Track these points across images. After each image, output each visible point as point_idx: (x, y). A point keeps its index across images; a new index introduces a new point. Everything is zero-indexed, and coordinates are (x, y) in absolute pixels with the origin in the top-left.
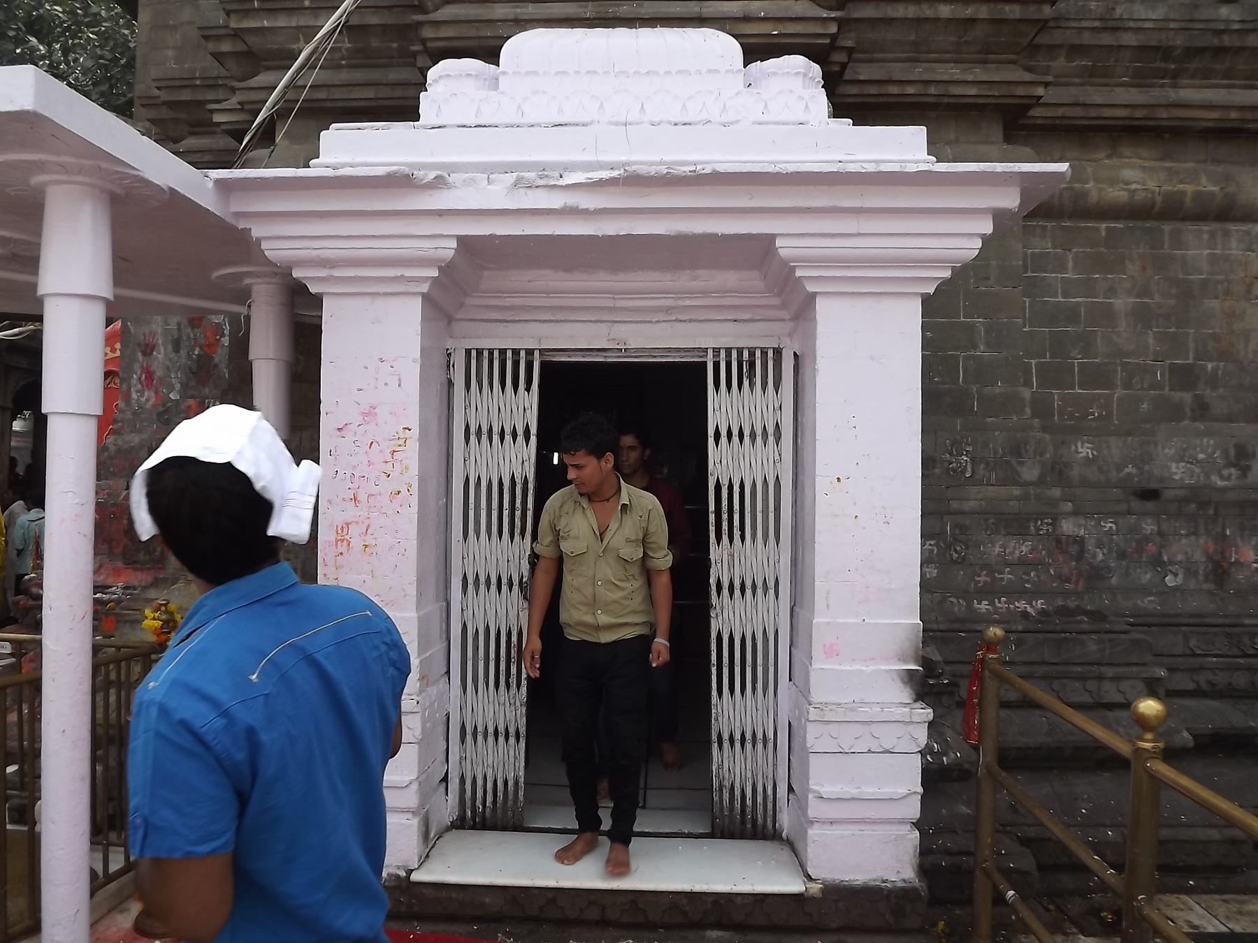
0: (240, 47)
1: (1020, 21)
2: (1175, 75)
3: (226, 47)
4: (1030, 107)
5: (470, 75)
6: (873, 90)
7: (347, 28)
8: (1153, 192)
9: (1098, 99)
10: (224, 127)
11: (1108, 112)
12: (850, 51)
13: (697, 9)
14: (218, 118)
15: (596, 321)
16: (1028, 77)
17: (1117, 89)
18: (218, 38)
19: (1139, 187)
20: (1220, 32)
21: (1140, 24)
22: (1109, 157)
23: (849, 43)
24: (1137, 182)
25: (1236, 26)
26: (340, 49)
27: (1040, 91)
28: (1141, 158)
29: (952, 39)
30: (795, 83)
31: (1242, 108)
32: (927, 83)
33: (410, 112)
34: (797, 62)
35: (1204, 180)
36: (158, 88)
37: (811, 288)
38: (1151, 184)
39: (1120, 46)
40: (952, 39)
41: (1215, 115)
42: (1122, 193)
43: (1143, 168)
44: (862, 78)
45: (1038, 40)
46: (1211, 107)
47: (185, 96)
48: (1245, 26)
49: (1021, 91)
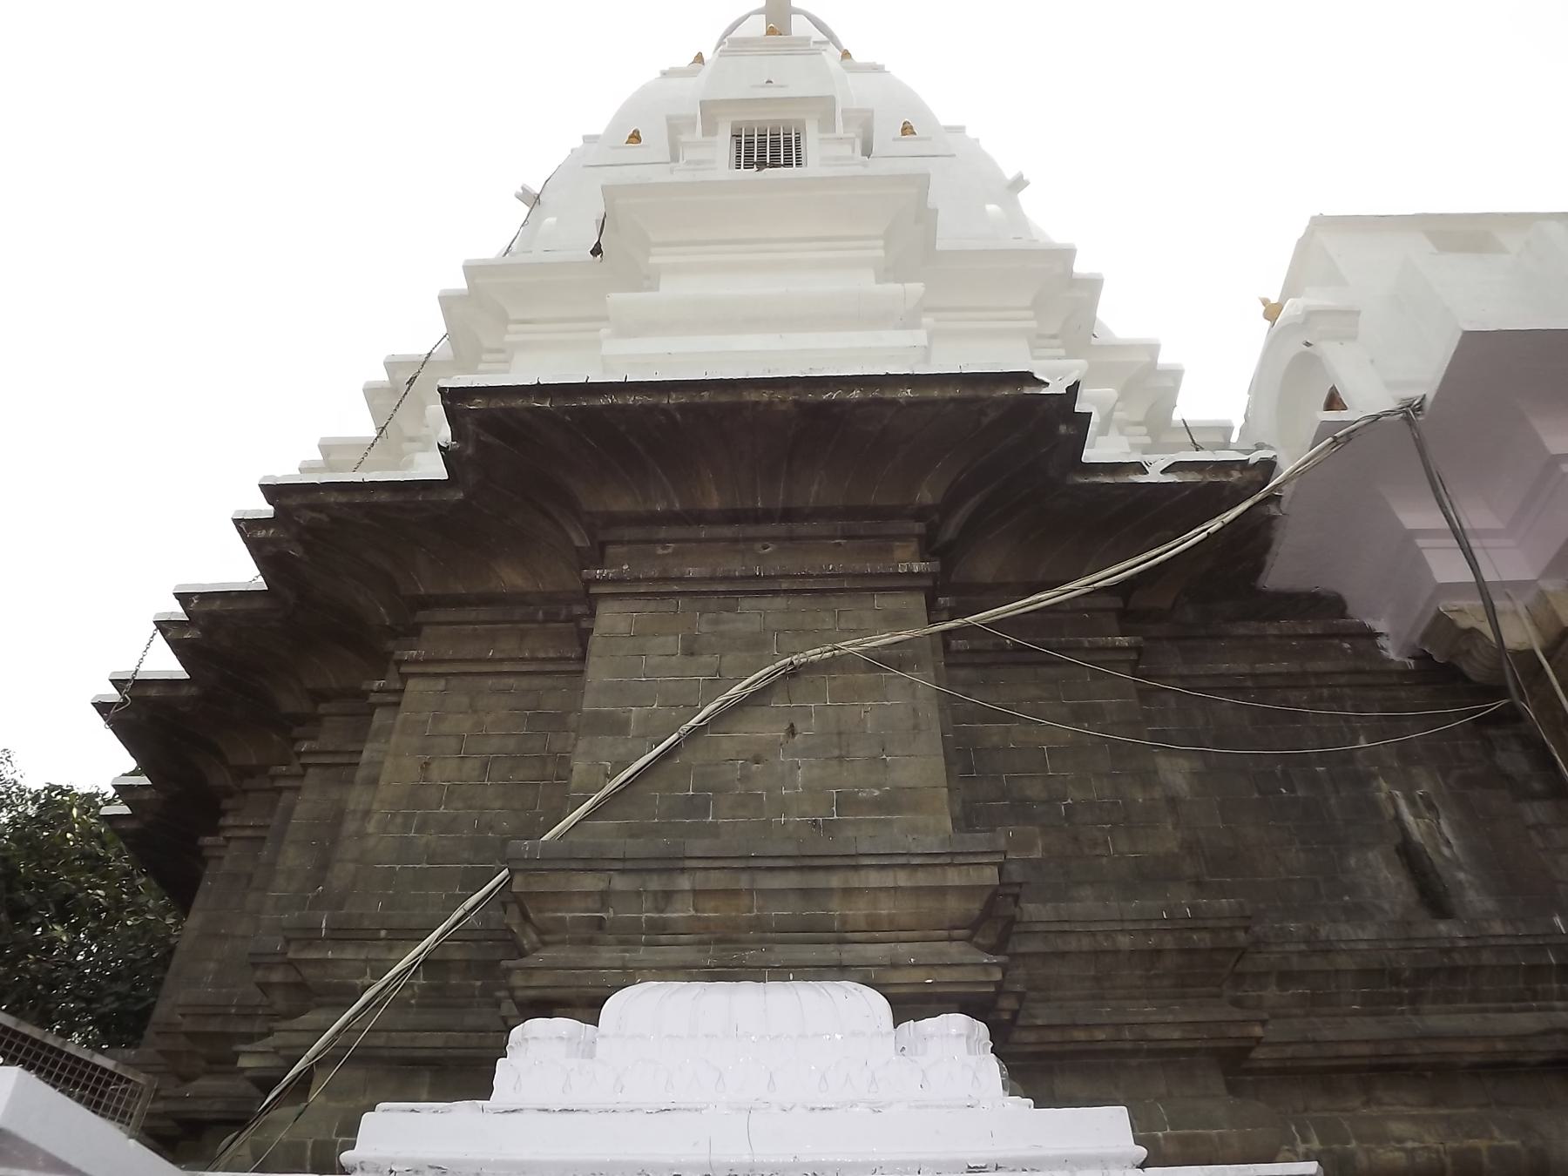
0: (292, 977)
1: (1212, 950)
2: (1414, 999)
3: (276, 977)
4: (1250, 1049)
5: (561, 1038)
6: (1054, 1036)
7: (428, 963)
8: (1438, 1151)
9: (1329, 1034)
10: (248, 1074)
11: (1346, 1050)
12: (1021, 997)
13: (835, 955)
14: (243, 1062)
15: (743, 869)
16: (1238, 1015)
17: (1348, 1019)
18: (270, 967)
19: (1416, 1145)
20: (1447, 952)
21: (1352, 945)
22: (1366, 1104)
23: (1019, 988)
24: (1414, 1140)
25: (1463, 944)
26: (412, 985)
27: (1258, 1031)
28: (1406, 1104)
29: (1138, 972)
30: (956, 1047)
31: (1507, 1038)
32: (1118, 1026)
33: (479, 1086)
34: (957, 1022)
35: (1497, 1133)
36: (183, 1015)
37: (1030, 314)
38: (1431, 1141)
39: (1337, 971)
40: (1138, 972)
41: (1479, 1047)
42: (1397, 1154)
43: (1413, 1119)
44: (1039, 1022)
45: (1239, 967)
46: (1467, 1037)
47: (214, 1026)
48: (1472, 943)
49: (1234, 1032)
